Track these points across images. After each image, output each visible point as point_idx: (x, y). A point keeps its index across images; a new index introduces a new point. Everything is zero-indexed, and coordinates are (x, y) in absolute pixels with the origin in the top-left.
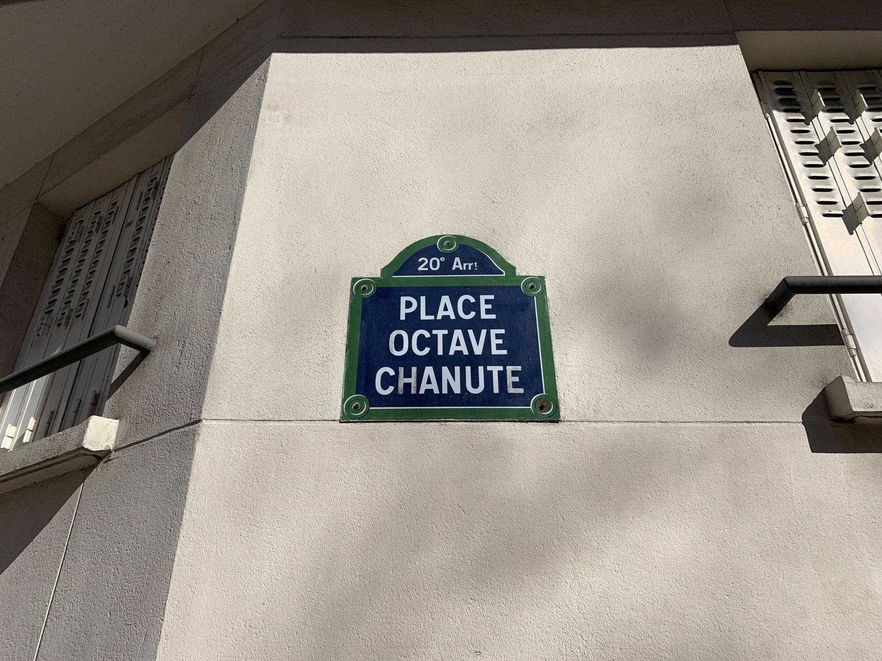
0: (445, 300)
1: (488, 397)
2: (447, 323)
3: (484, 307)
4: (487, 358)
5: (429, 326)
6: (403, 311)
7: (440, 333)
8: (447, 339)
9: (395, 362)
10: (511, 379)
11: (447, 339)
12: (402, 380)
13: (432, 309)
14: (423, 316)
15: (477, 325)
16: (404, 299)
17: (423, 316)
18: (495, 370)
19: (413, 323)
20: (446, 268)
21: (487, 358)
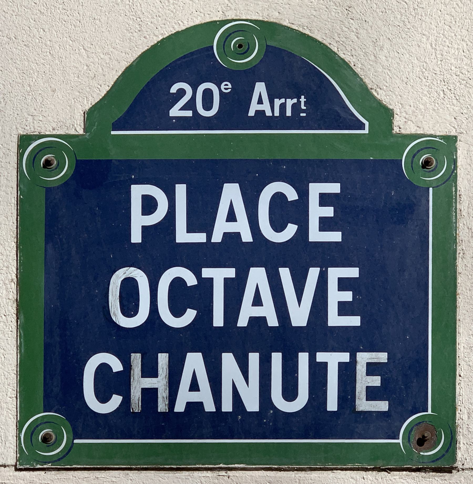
0: (231, 193)
1: (314, 421)
2: (233, 252)
3: (316, 212)
4: (318, 335)
5: (196, 257)
6: (138, 222)
7: (219, 275)
8: (234, 290)
9: (122, 343)
10: (364, 381)
11: (234, 290)
12: (139, 383)
13: (201, 217)
14: (183, 236)
15: (301, 255)
16: (138, 192)
17: (183, 236)
18: (333, 360)
19: (159, 249)
20: (234, 111)
21: (318, 335)
